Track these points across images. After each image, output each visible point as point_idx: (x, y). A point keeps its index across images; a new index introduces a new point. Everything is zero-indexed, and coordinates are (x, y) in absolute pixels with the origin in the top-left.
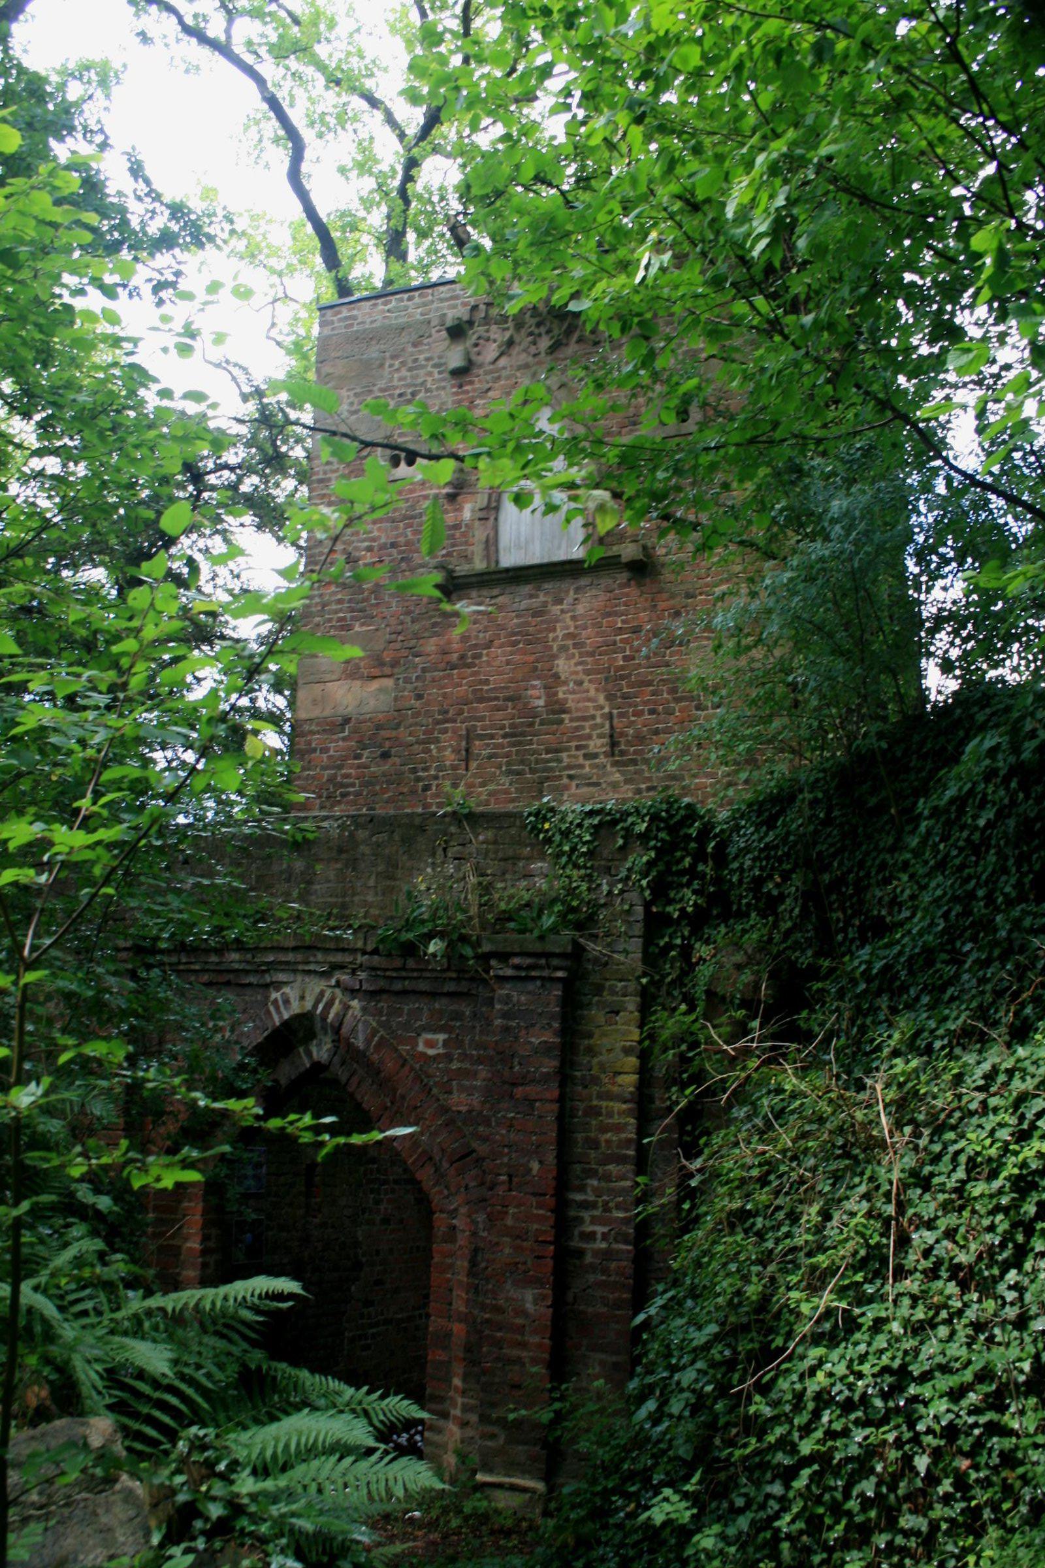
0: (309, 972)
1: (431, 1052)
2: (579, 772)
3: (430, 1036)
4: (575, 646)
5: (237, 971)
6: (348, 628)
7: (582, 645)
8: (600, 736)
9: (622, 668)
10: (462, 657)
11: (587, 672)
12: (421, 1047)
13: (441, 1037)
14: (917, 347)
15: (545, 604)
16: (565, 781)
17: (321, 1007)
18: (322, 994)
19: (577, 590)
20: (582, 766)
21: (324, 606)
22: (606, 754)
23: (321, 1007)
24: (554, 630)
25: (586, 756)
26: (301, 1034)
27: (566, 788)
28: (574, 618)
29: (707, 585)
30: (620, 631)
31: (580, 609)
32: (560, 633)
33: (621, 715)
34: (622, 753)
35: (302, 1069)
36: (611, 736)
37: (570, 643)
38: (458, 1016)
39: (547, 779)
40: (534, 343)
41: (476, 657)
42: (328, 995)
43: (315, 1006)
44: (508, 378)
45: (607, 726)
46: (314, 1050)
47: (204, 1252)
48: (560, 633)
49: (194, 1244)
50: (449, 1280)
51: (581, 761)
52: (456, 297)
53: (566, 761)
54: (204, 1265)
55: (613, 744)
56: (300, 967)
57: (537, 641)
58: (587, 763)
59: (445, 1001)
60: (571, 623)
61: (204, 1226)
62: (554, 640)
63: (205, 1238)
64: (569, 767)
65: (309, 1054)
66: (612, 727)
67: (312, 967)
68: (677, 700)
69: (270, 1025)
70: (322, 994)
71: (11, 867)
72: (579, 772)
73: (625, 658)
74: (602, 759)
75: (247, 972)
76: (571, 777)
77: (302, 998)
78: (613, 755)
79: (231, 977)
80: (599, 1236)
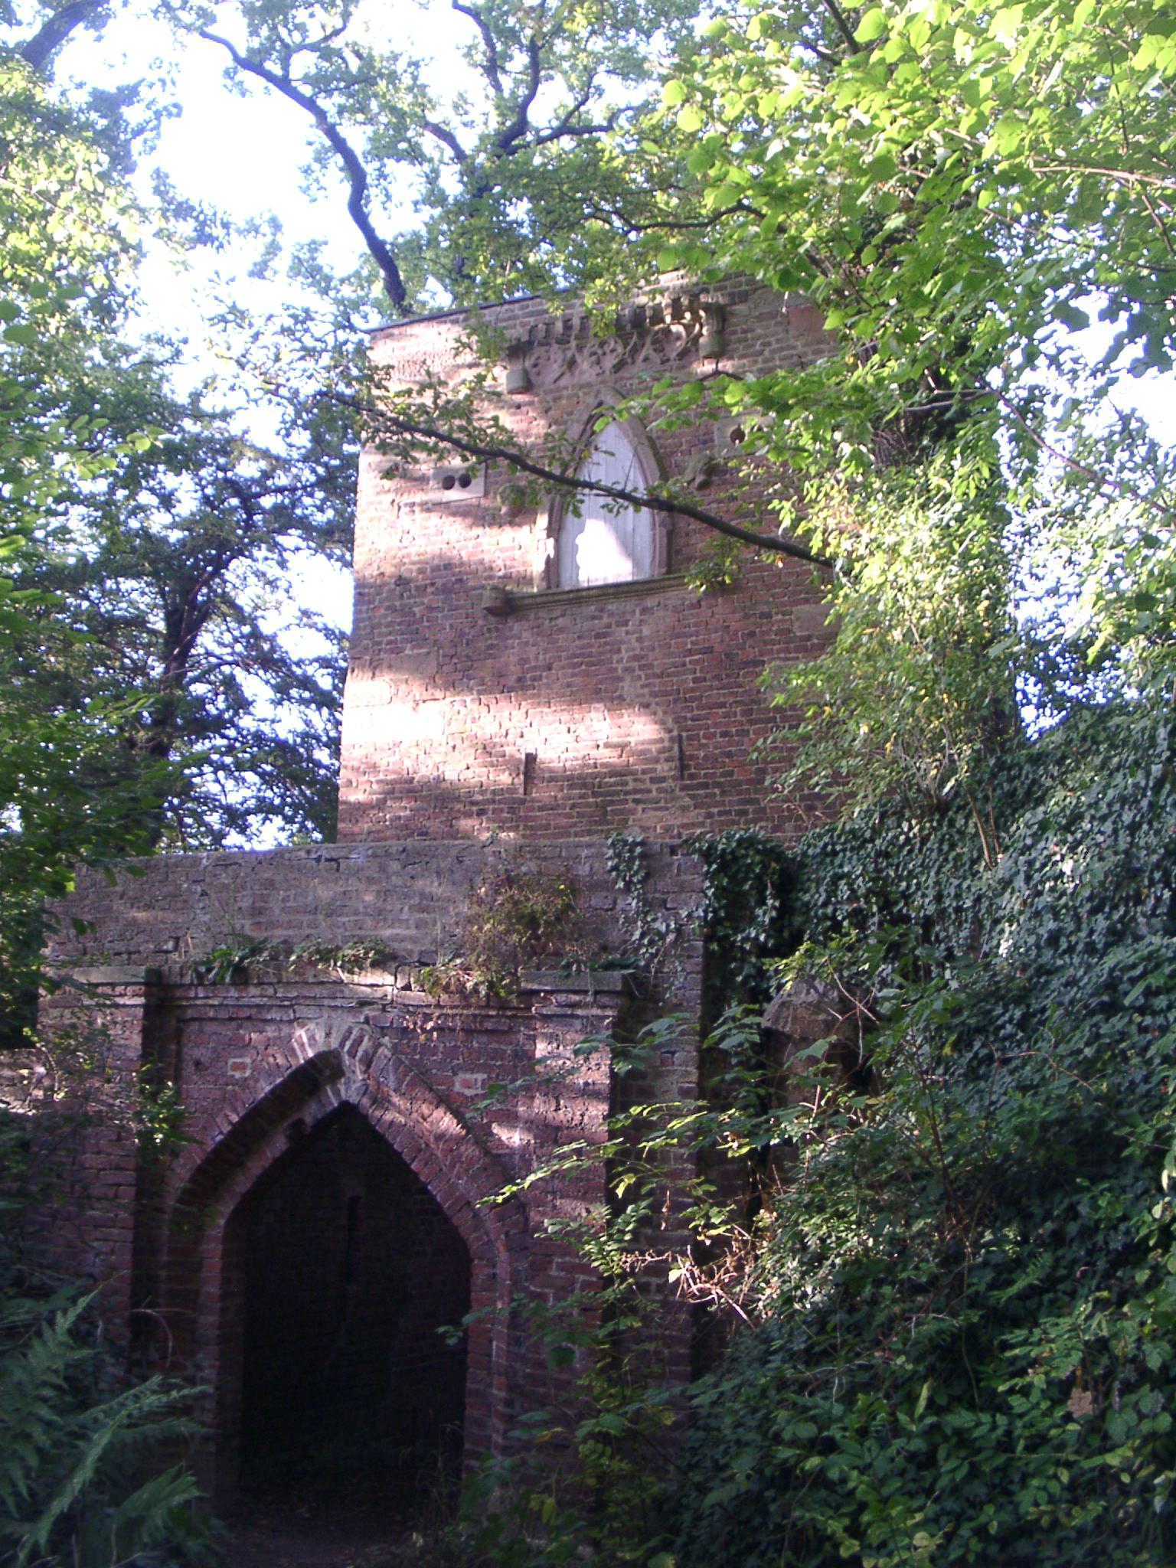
0: (335, 1007)
1: (469, 1092)
2: (645, 796)
3: (468, 1076)
4: (641, 668)
5: (258, 1006)
6: (401, 651)
7: (650, 666)
8: (667, 760)
9: (692, 690)
10: (520, 680)
11: (654, 695)
12: (457, 1088)
13: (481, 1076)
14: (643, 1501)
15: (609, 626)
16: (631, 805)
17: (348, 1044)
18: (350, 1031)
19: (644, 611)
20: (649, 791)
21: (373, 628)
22: (674, 778)
23: (348, 1044)
24: (619, 651)
25: (653, 780)
26: (328, 1072)
27: (633, 812)
28: (640, 640)
29: (784, 605)
30: (690, 652)
31: (646, 631)
32: (625, 655)
33: (689, 738)
34: (692, 777)
35: (329, 1109)
36: (681, 759)
37: (636, 664)
38: (498, 1055)
39: (612, 802)
40: (598, 362)
41: (534, 679)
42: (355, 1032)
43: (342, 1045)
44: (569, 397)
45: (676, 748)
46: (342, 1088)
47: (224, 1296)
48: (625, 655)
49: (213, 1289)
50: (489, 1331)
51: (648, 785)
52: (516, 317)
53: (631, 786)
54: (223, 1311)
55: (683, 767)
56: (326, 1002)
57: (600, 663)
58: (654, 787)
59: (484, 1039)
60: (637, 645)
61: (223, 1269)
62: (620, 661)
63: (226, 1281)
64: (635, 791)
65: (337, 1093)
66: (681, 751)
67: (338, 1002)
68: (752, 722)
69: (293, 1062)
70: (350, 1031)
71: (265, 853)
72: (645, 796)
73: (695, 680)
74: (670, 783)
75: (270, 1007)
76: (637, 801)
77: (328, 1035)
78: (682, 777)
79: (254, 1011)
80: (653, 1287)
